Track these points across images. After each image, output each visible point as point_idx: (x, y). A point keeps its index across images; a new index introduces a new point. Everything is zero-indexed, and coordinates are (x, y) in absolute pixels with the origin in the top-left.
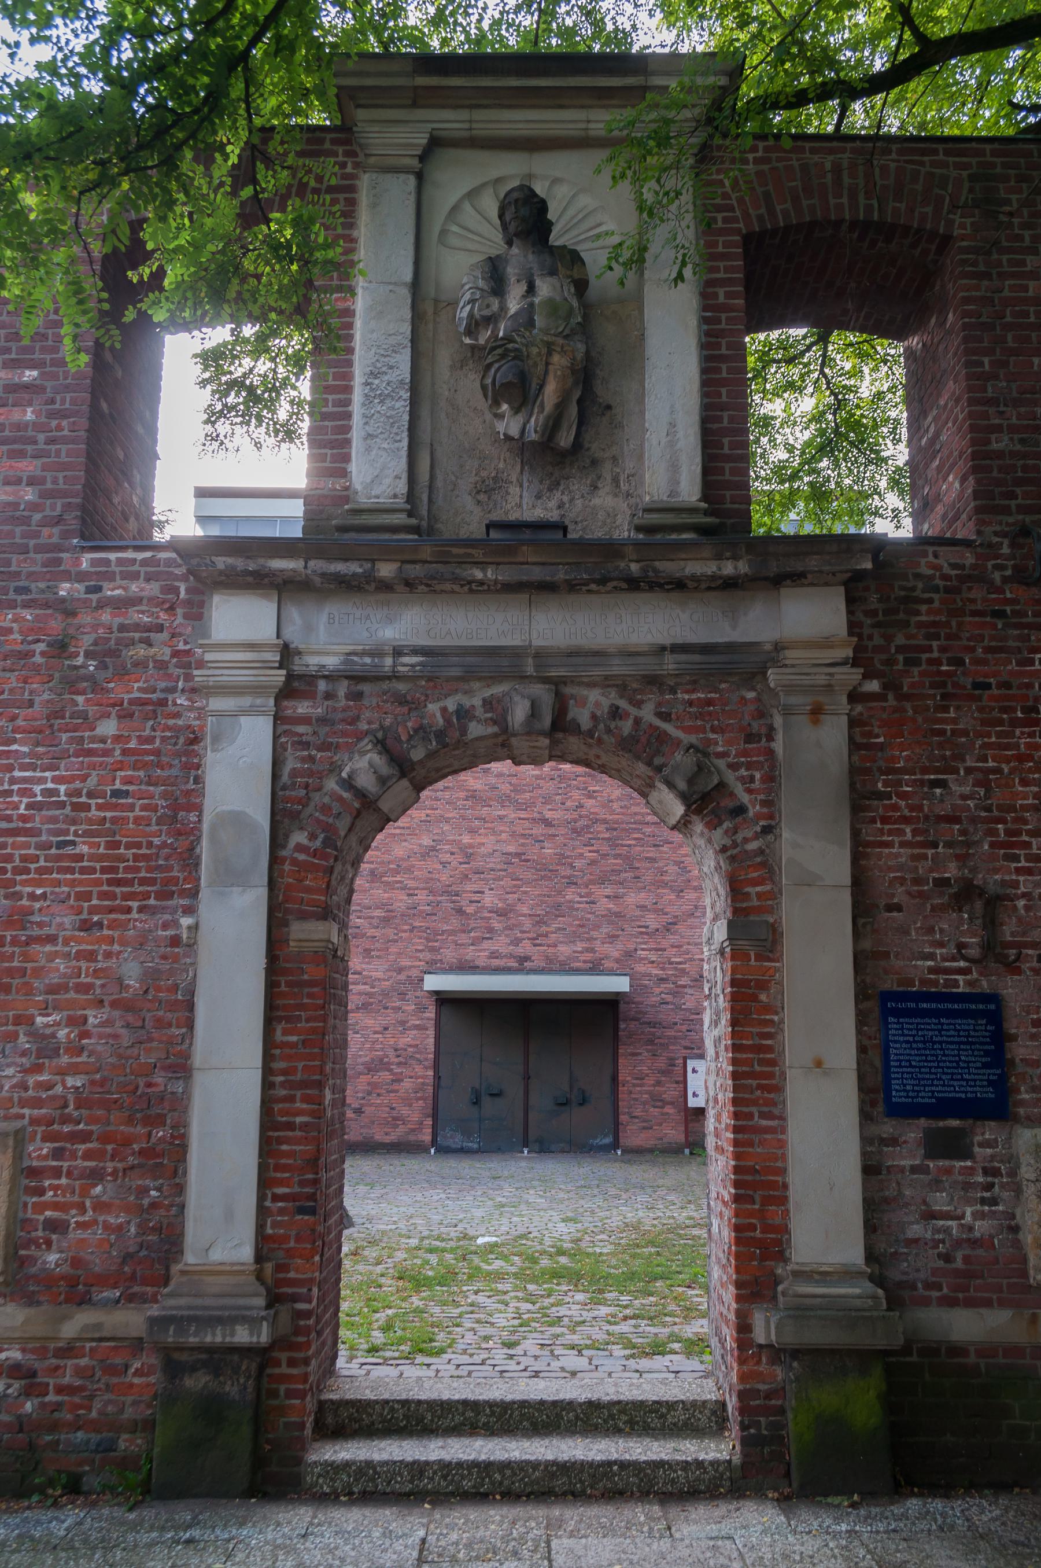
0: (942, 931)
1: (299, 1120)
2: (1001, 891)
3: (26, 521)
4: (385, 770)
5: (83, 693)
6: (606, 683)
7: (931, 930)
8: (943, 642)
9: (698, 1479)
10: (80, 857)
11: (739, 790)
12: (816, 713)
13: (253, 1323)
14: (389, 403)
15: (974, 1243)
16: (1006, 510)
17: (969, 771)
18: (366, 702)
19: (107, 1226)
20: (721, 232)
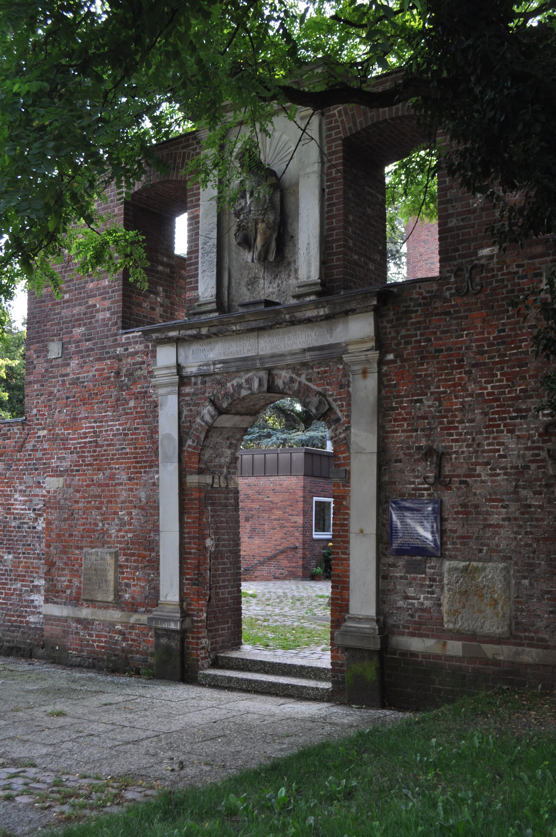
0: (418, 471)
1: (193, 551)
2: (445, 451)
3: (107, 325)
4: (213, 413)
5: (124, 391)
6: (287, 367)
7: (413, 471)
8: (422, 331)
9: (317, 694)
10: (127, 454)
11: (338, 411)
12: (365, 373)
13: (175, 622)
14: (210, 255)
15: (423, 610)
16: (454, 259)
17: (432, 393)
18: (207, 385)
19: (140, 586)
20: (334, 140)
